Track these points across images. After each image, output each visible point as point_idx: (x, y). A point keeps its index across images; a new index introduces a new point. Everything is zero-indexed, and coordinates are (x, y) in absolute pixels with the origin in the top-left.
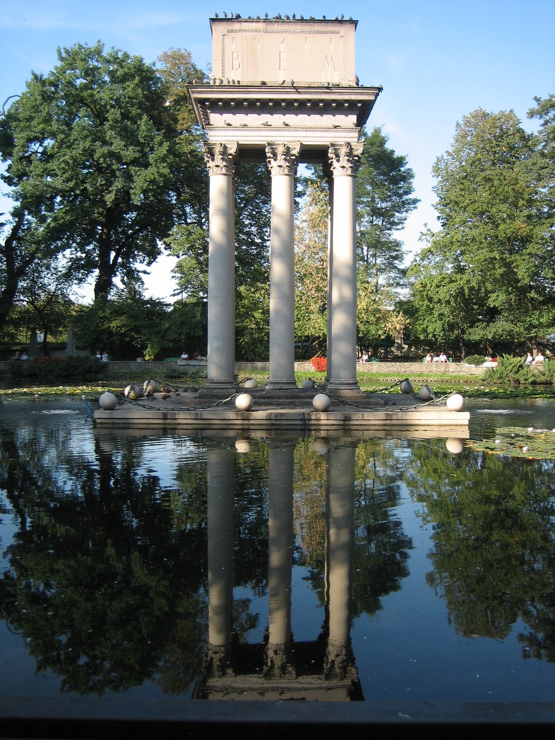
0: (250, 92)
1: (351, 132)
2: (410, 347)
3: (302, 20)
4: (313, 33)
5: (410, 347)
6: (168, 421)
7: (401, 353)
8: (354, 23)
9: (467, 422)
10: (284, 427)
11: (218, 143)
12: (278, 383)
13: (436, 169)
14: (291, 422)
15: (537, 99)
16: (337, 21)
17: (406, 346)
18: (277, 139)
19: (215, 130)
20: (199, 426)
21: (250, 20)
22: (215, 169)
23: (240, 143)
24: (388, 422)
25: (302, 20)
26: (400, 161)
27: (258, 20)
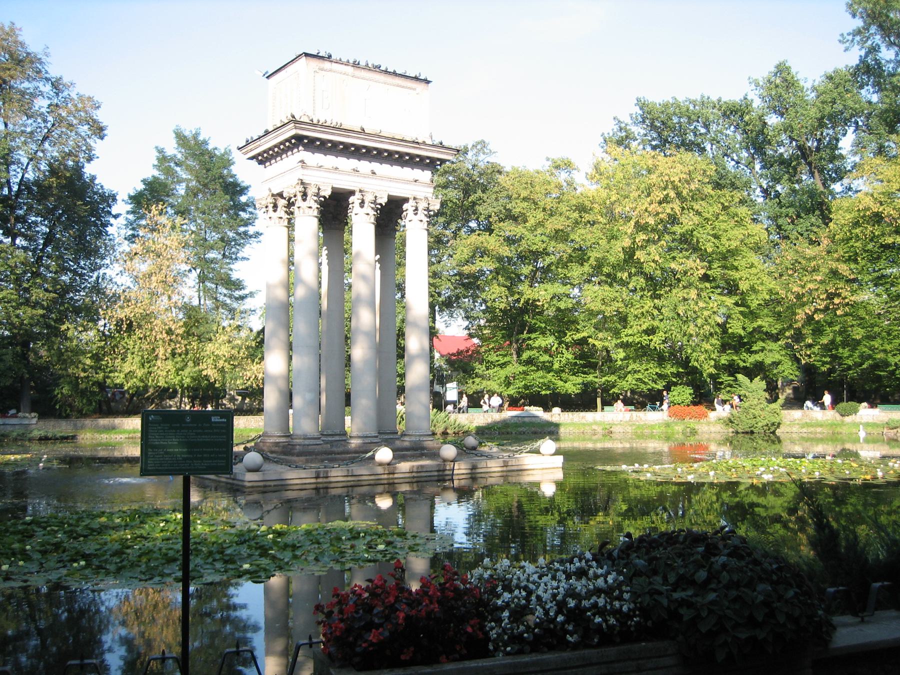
0: (349, 136)
2: (244, 399)
3: (386, 72)
4: (394, 85)
5: (244, 399)
6: (320, 480)
7: (234, 404)
10: (423, 479)
11: (313, 183)
12: (367, 437)
16: (416, 79)
17: (240, 398)
20: (349, 484)
22: (308, 210)
24: (505, 469)
27: (347, 63)
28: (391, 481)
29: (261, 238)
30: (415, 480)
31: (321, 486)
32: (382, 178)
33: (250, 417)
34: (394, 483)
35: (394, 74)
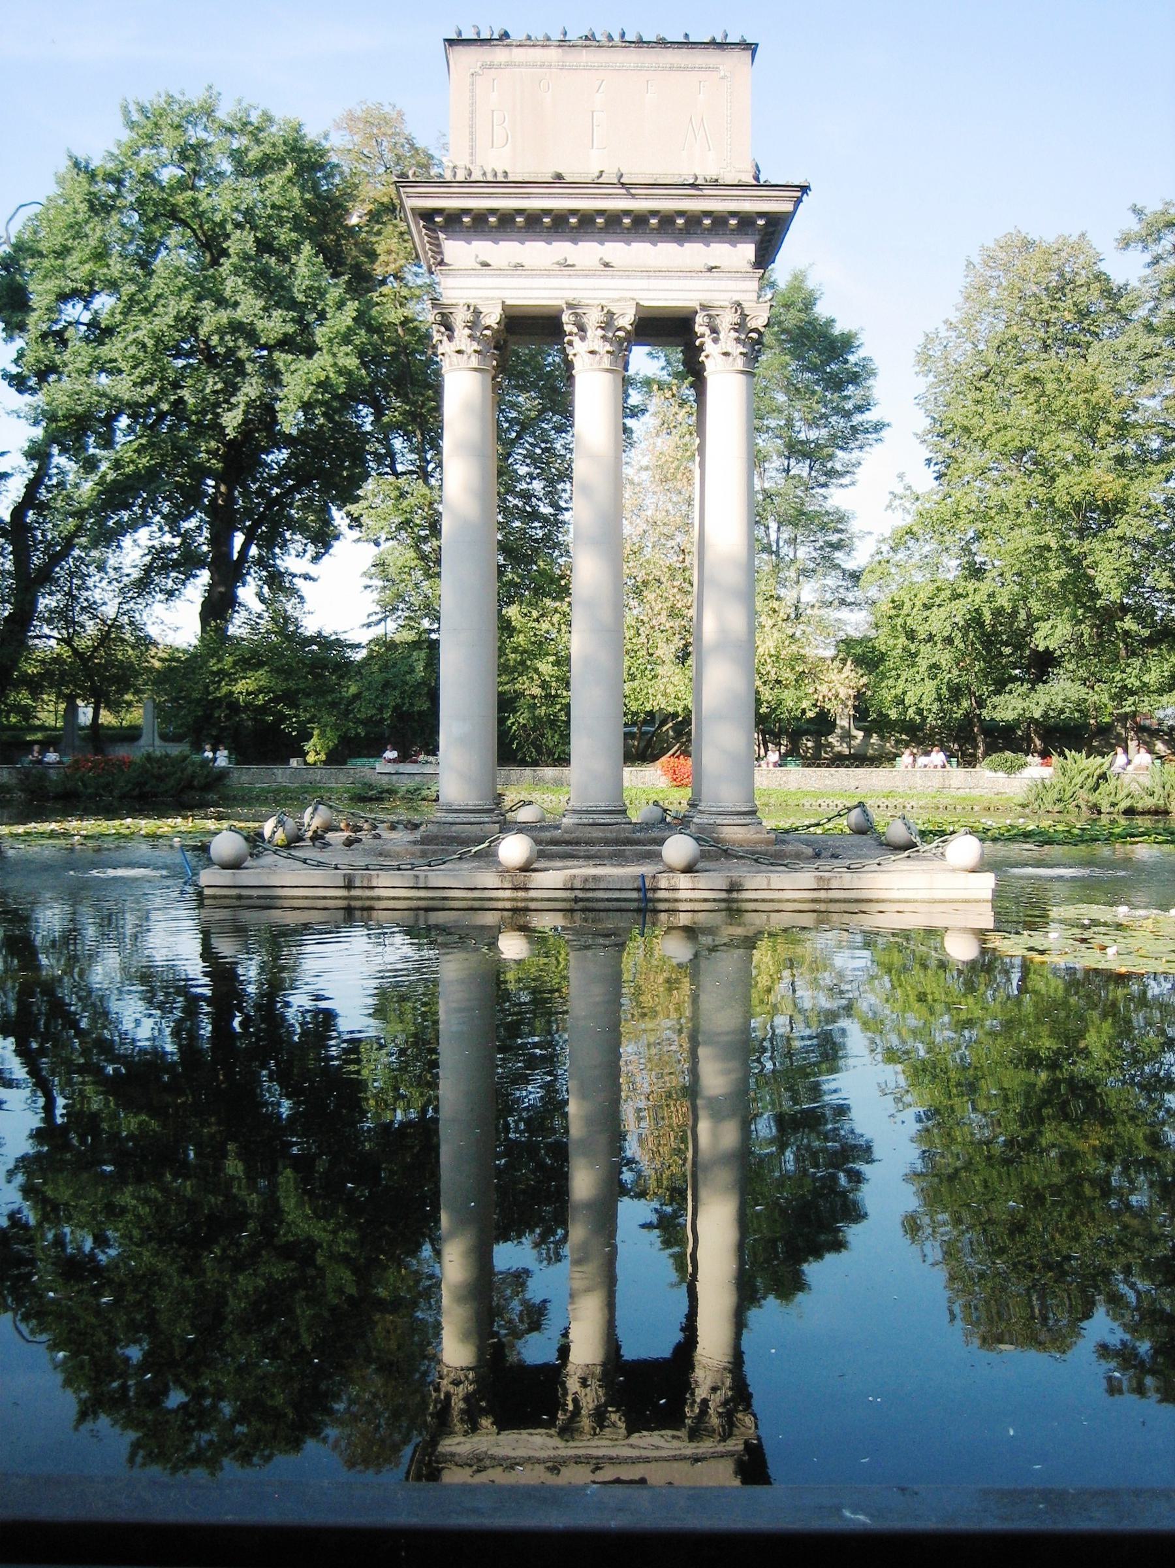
0: (528, 196)
1: (744, 279)
2: (868, 735)
3: (640, 43)
5: (868, 735)
6: (354, 893)
8: (751, 48)
9: (988, 895)
11: (462, 302)
12: (587, 812)
13: (924, 359)
14: (617, 895)
15: (1137, 211)
17: (860, 734)
18: (717, 295)
19: (455, 276)
20: (422, 904)
21: (529, 42)
23: (508, 302)
25: (640, 43)
26: (846, 344)
27: (546, 43)
28: (521, 905)
29: (883, 434)
30: (581, 905)
31: (358, 904)
32: (628, 273)
33: (861, 771)
34: (371, 908)
35: (663, 43)
